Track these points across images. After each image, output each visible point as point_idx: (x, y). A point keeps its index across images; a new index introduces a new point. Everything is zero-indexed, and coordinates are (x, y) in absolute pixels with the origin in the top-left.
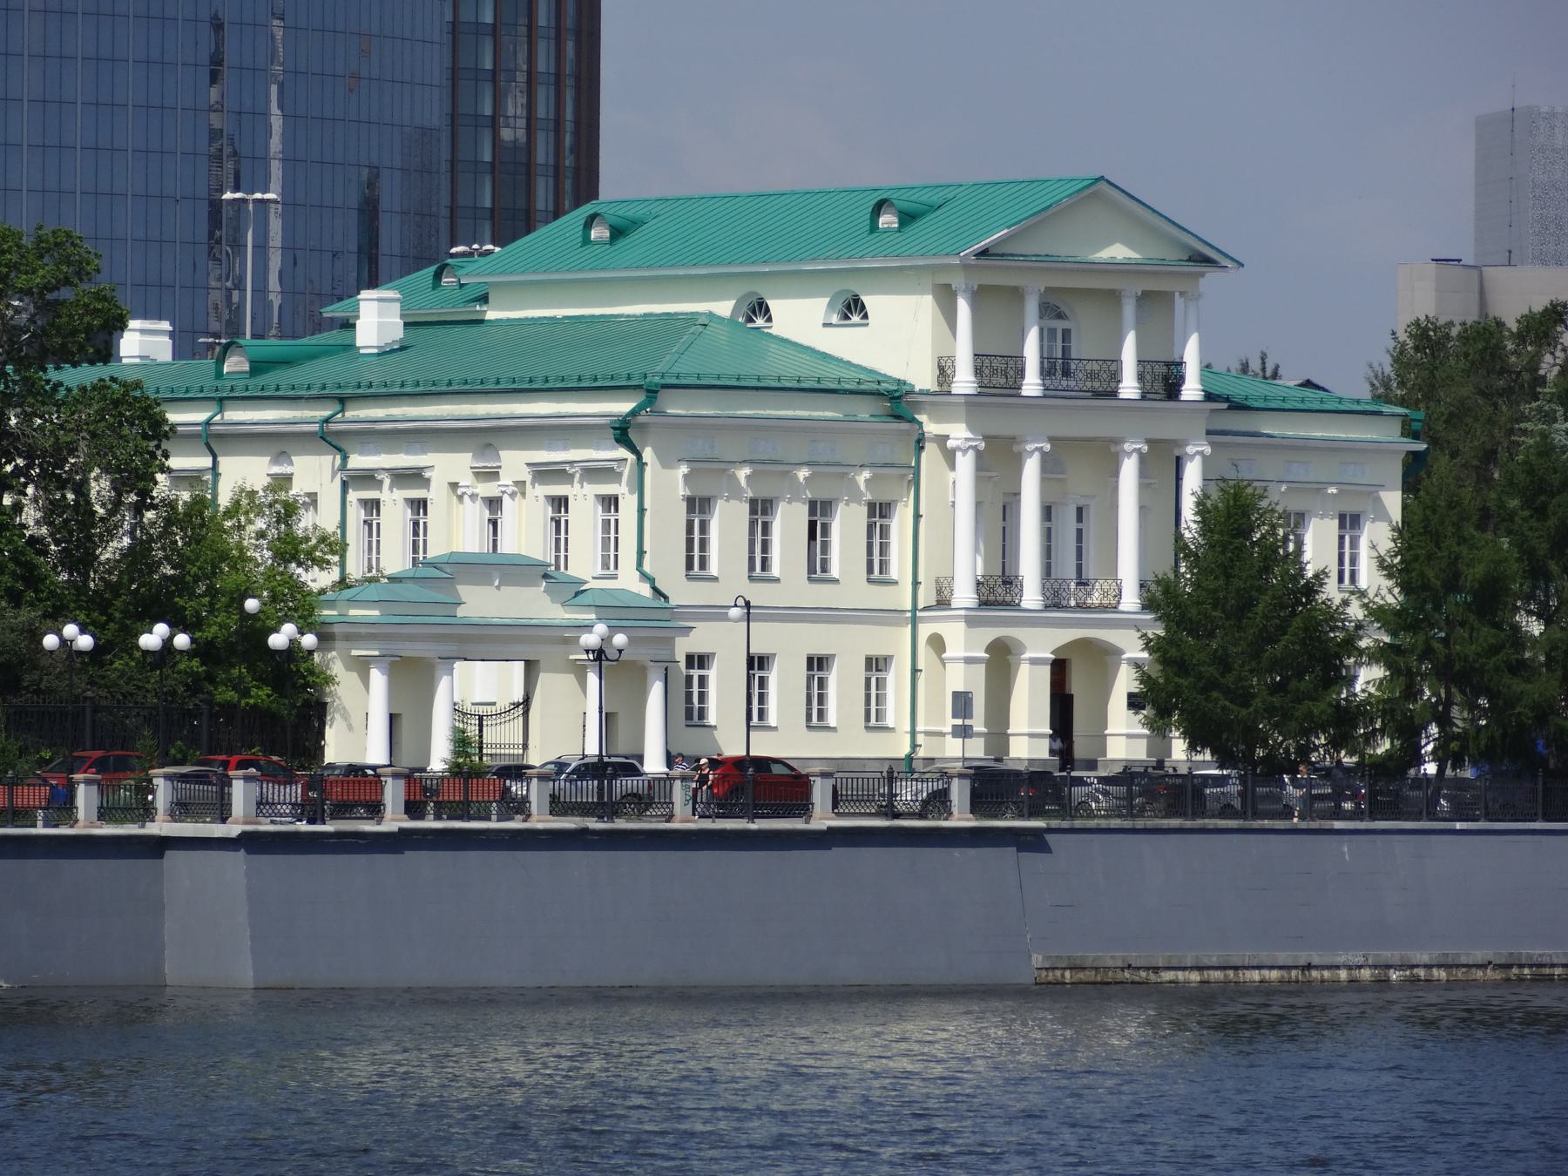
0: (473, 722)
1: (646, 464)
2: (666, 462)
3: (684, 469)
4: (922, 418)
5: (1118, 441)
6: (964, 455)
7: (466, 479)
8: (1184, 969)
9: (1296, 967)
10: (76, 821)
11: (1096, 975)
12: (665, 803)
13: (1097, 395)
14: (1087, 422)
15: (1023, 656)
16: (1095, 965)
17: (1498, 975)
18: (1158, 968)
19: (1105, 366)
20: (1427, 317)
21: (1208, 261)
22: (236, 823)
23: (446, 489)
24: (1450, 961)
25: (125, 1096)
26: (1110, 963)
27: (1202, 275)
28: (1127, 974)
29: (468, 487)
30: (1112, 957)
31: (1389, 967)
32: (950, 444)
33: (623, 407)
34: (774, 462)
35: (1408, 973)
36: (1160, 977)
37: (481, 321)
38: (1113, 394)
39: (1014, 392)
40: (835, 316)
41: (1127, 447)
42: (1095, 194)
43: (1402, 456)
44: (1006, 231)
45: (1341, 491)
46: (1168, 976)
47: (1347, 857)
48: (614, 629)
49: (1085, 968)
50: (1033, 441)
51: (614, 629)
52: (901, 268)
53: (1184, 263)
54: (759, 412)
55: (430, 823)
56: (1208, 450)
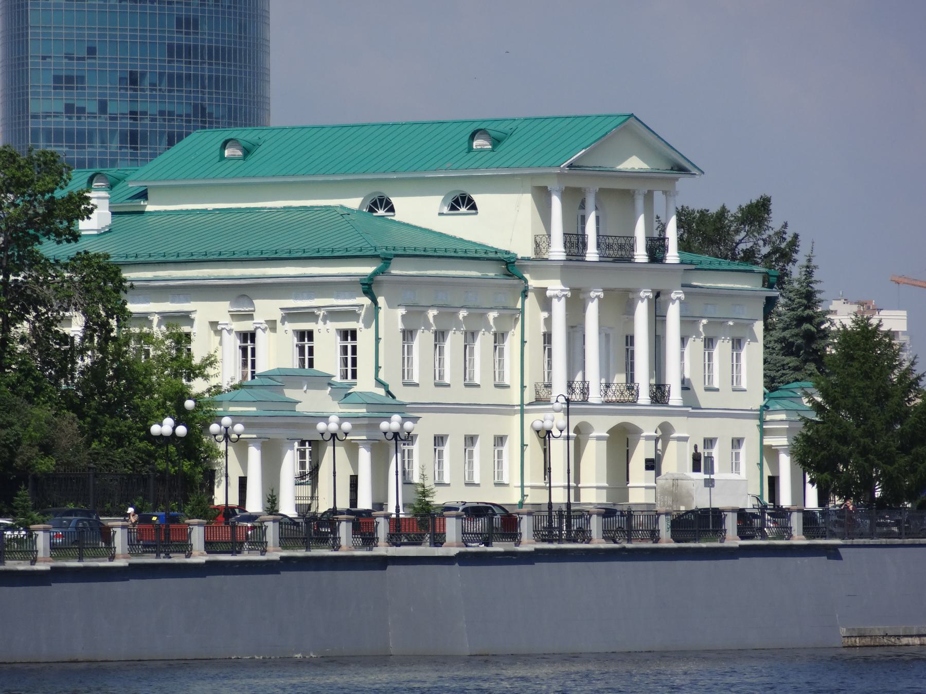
1: (380, 308)
2: (391, 305)
3: (402, 311)
4: (527, 276)
5: (639, 291)
6: (559, 301)
7: (224, 319)
8: (911, 636)
10: (340, 547)
11: (871, 641)
13: (617, 260)
14: (620, 279)
15: (672, 436)
18: (899, 636)
20: (683, 206)
21: (682, 169)
22: (451, 545)
23: (207, 326)
26: (877, 633)
27: (677, 179)
29: (227, 324)
32: (549, 293)
33: (367, 270)
36: (901, 642)
37: (142, 213)
38: (629, 259)
39: (580, 258)
40: (446, 208)
41: (593, 294)
44: (584, 151)
45: (735, 324)
46: (905, 641)
48: (177, 423)
49: (865, 636)
51: (177, 423)
52: (513, 176)
53: (667, 172)
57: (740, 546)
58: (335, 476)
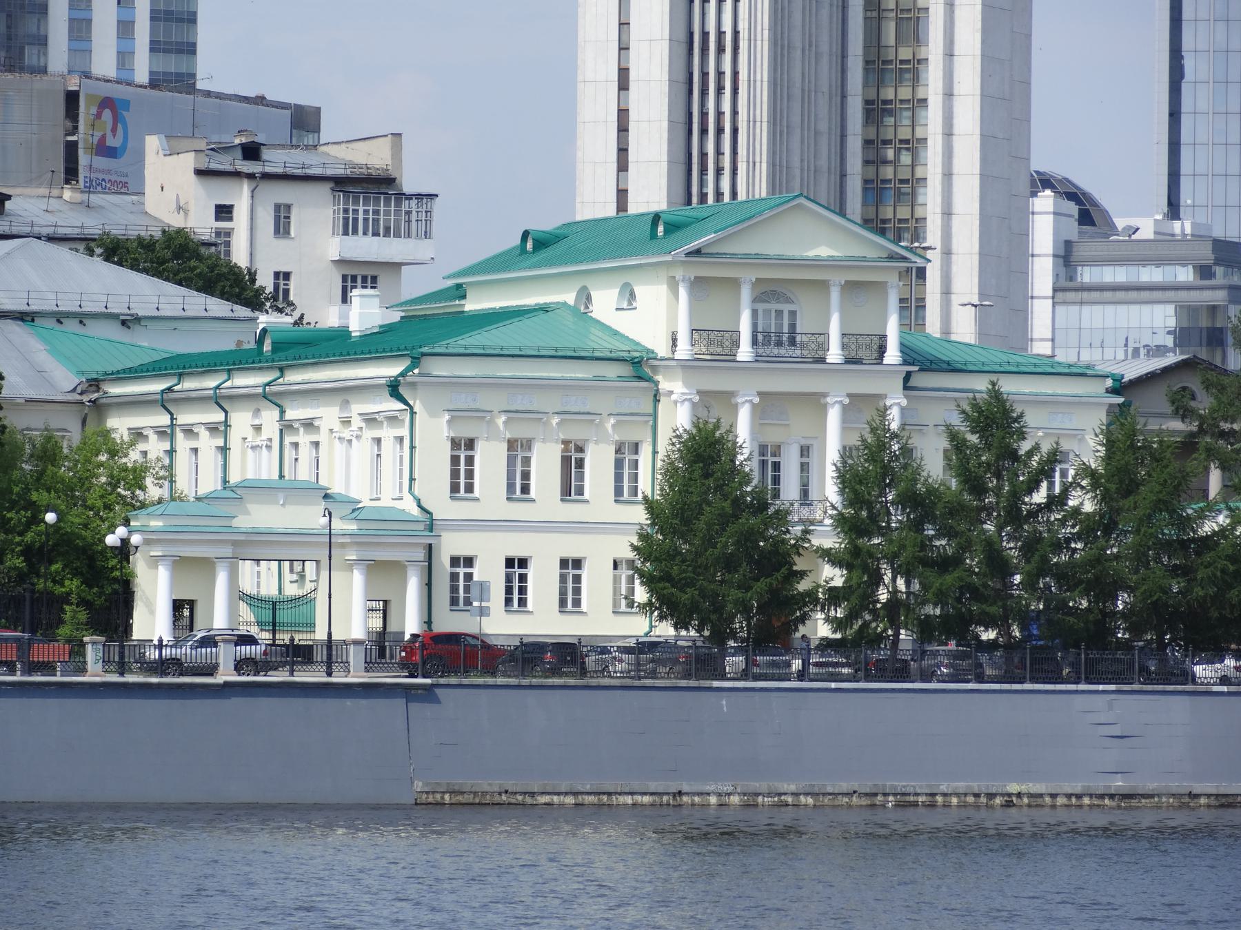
0: (267, 606)
1: (416, 413)
2: (433, 414)
3: (447, 417)
4: (659, 378)
8: (559, 794)
9: (668, 794)
11: (474, 798)
12: (391, 663)
16: (473, 790)
17: (865, 801)
18: (534, 793)
19: (813, 338)
24: (816, 790)
25: (960, 867)
28: (504, 797)
30: (490, 784)
31: (757, 795)
34: (589, 413)
35: (776, 799)
36: (536, 800)
38: (822, 360)
42: (799, 206)
43: (1106, 407)
44: (713, 235)
47: (725, 709)
50: (744, 395)
54: (565, 375)
55: (130, 678)
56: (904, 402)
57: (225, 682)
58: (330, 597)
